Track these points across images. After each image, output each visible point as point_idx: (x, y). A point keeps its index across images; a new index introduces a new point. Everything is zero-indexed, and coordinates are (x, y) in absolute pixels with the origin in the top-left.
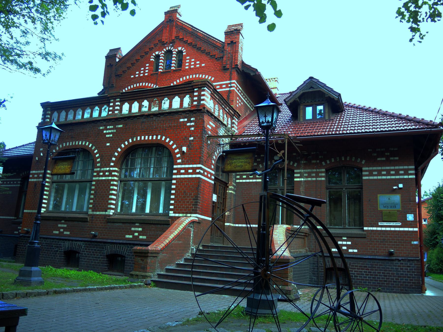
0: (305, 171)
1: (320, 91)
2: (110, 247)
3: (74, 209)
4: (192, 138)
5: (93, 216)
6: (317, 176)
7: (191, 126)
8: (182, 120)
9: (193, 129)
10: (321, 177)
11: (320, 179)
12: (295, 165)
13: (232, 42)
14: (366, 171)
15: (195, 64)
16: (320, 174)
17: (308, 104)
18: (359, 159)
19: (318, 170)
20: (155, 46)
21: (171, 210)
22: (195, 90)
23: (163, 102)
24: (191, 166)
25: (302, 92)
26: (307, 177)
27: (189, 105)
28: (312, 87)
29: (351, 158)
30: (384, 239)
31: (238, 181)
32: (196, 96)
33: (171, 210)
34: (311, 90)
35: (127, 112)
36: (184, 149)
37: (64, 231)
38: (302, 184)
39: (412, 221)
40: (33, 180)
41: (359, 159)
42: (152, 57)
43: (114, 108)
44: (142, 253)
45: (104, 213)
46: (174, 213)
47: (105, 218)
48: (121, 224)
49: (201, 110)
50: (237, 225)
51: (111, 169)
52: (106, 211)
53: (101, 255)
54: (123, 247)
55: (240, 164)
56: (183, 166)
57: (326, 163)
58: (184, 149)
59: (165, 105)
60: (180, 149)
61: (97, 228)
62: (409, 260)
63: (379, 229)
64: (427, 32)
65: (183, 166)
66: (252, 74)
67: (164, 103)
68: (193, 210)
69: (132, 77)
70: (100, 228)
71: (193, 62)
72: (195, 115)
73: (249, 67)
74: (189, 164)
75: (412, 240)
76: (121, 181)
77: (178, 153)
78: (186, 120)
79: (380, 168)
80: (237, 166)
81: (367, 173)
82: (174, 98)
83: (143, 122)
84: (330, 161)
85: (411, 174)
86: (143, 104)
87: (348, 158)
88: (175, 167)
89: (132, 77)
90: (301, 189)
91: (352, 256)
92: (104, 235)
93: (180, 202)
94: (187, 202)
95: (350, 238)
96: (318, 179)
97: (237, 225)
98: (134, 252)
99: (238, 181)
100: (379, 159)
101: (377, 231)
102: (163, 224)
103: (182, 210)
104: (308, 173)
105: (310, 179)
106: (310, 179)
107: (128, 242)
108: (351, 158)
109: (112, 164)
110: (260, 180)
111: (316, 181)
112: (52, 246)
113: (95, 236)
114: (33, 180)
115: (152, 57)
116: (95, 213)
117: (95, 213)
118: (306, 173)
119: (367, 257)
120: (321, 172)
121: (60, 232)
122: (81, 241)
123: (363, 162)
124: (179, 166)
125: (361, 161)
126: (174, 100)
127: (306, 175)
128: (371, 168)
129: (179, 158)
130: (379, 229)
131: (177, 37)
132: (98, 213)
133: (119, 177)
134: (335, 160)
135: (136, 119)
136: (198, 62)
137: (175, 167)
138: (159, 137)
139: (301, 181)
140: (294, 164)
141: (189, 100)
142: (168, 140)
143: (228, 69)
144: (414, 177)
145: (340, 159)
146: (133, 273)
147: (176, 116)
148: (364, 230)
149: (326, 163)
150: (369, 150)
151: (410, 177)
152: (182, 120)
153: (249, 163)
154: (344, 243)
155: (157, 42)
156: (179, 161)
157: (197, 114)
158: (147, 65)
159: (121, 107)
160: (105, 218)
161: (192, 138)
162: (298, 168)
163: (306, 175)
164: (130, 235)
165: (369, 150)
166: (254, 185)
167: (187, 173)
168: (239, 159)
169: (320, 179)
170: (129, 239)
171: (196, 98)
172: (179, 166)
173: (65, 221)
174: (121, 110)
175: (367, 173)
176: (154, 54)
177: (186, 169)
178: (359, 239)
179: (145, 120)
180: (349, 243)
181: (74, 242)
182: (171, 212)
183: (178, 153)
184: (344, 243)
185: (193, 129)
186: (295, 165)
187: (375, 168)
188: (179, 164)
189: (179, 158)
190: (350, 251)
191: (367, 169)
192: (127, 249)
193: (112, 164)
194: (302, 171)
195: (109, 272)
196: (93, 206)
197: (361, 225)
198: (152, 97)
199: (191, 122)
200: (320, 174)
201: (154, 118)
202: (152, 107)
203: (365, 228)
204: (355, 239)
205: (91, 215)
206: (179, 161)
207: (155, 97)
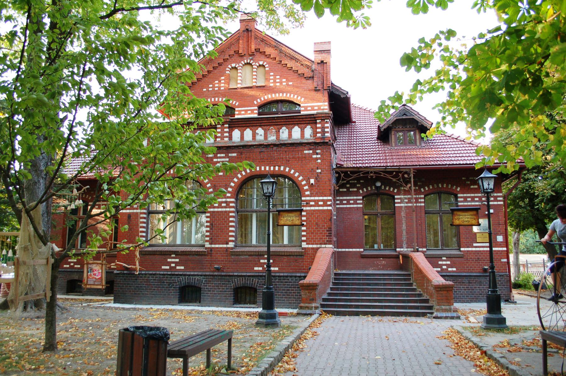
0: (405, 196)
1: (413, 119)
2: (237, 280)
3: (178, 242)
4: (319, 171)
5: (211, 249)
6: (417, 202)
7: (317, 159)
8: (306, 152)
9: (319, 161)
10: (421, 202)
11: (420, 204)
12: (395, 191)
13: (322, 62)
14: (461, 197)
15: (281, 83)
16: (419, 200)
17: (399, 129)
18: (450, 185)
19: (417, 196)
20: (230, 58)
21: (304, 241)
22: (318, 121)
23: (281, 131)
24: (321, 198)
25: (395, 119)
26: (407, 203)
27: (311, 136)
28: (405, 114)
29: (447, 186)
30: (478, 258)
31: (338, 206)
32: (319, 128)
33: (304, 241)
34: (404, 117)
35: (239, 140)
36: (312, 181)
37: (176, 266)
38: (403, 209)
39: (501, 242)
40: (124, 211)
41: (450, 185)
42: (227, 69)
43: (222, 134)
44: (310, 286)
45: (225, 246)
46: (307, 244)
47: (227, 251)
48: (247, 257)
49: (327, 142)
50: (340, 250)
51: (228, 200)
52: (227, 244)
53: (227, 289)
54: (253, 280)
55: (467, 220)
56: (312, 198)
57: (424, 189)
58: (312, 181)
59: (284, 134)
60: (308, 181)
61: (219, 261)
62: (500, 275)
63: (474, 249)
64: (464, 37)
65: (312, 198)
66: (342, 96)
67: (283, 132)
68: (327, 241)
69: (205, 90)
70: (222, 261)
71: (278, 79)
72: (320, 147)
73: (338, 89)
74: (319, 196)
75: (502, 258)
76: (238, 212)
77: (305, 185)
78: (311, 152)
79: (473, 195)
80: (464, 221)
81: (462, 199)
82: (293, 127)
83: (260, 152)
84: (429, 187)
85: (500, 201)
86: (257, 131)
87: (450, 186)
88: (303, 198)
89: (205, 90)
90: (402, 213)
91: (452, 274)
92: (228, 268)
93: (312, 233)
94: (320, 233)
95: (449, 257)
96: (418, 204)
97: (340, 250)
98: (301, 286)
99: (338, 206)
100: (472, 187)
101: (472, 251)
102: (284, 255)
103: (315, 241)
104: (409, 198)
105: (410, 205)
106: (410, 205)
107: (257, 274)
108: (447, 186)
109: (229, 195)
110: (361, 206)
111: (416, 206)
112: (164, 282)
113: (218, 270)
114: (124, 211)
115: (227, 69)
116: (213, 246)
117: (213, 246)
118: (406, 198)
119: (464, 274)
120: (421, 198)
121: (171, 268)
122: (201, 275)
123: (459, 189)
124: (308, 198)
125: (457, 188)
126: (293, 130)
127: (406, 201)
128: (465, 195)
129: (307, 190)
130: (474, 249)
131: (257, 50)
132: (217, 246)
133: (236, 207)
134: (433, 186)
135: (252, 147)
136: (278, 77)
137: (303, 198)
138: (282, 168)
139: (401, 207)
140: (394, 190)
141: (311, 131)
142: (292, 172)
143: (319, 90)
144: (502, 203)
145: (438, 186)
146: (302, 305)
147: (300, 148)
148: (461, 251)
149: (424, 189)
150: (463, 178)
151: (499, 203)
152: (306, 152)
153: (475, 219)
154: (444, 263)
155: (232, 53)
156: (308, 193)
157: (322, 146)
158: (223, 78)
159: (230, 133)
160: (227, 251)
161: (319, 171)
162: (398, 194)
163: (406, 201)
164: (258, 267)
165: (463, 178)
166: (355, 210)
167: (317, 205)
168: (465, 215)
169: (420, 204)
170: (258, 271)
171: (319, 130)
172: (308, 198)
173: (176, 255)
174: (230, 137)
175: (462, 199)
176: (230, 66)
177: (316, 202)
178: (457, 259)
179: (263, 150)
180: (449, 263)
181: (191, 277)
182: (303, 243)
183: (305, 185)
184: (444, 263)
185: (319, 161)
186: (395, 191)
187: (469, 195)
188: (308, 196)
189: (307, 190)
190: (450, 269)
191: (462, 195)
192: (258, 281)
193: (229, 195)
194: (403, 197)
195: (235, 306)
196: (211, 239)
197: (459, 246)
198: (267, 125)
199: (317, 154)
200: (419, 200)
201: (275, 148)
202: (269, 135)
203: (462, 249)
204: (454, 259)
205: (209, 248)
206: (308, 193)
207: (271, 125)
